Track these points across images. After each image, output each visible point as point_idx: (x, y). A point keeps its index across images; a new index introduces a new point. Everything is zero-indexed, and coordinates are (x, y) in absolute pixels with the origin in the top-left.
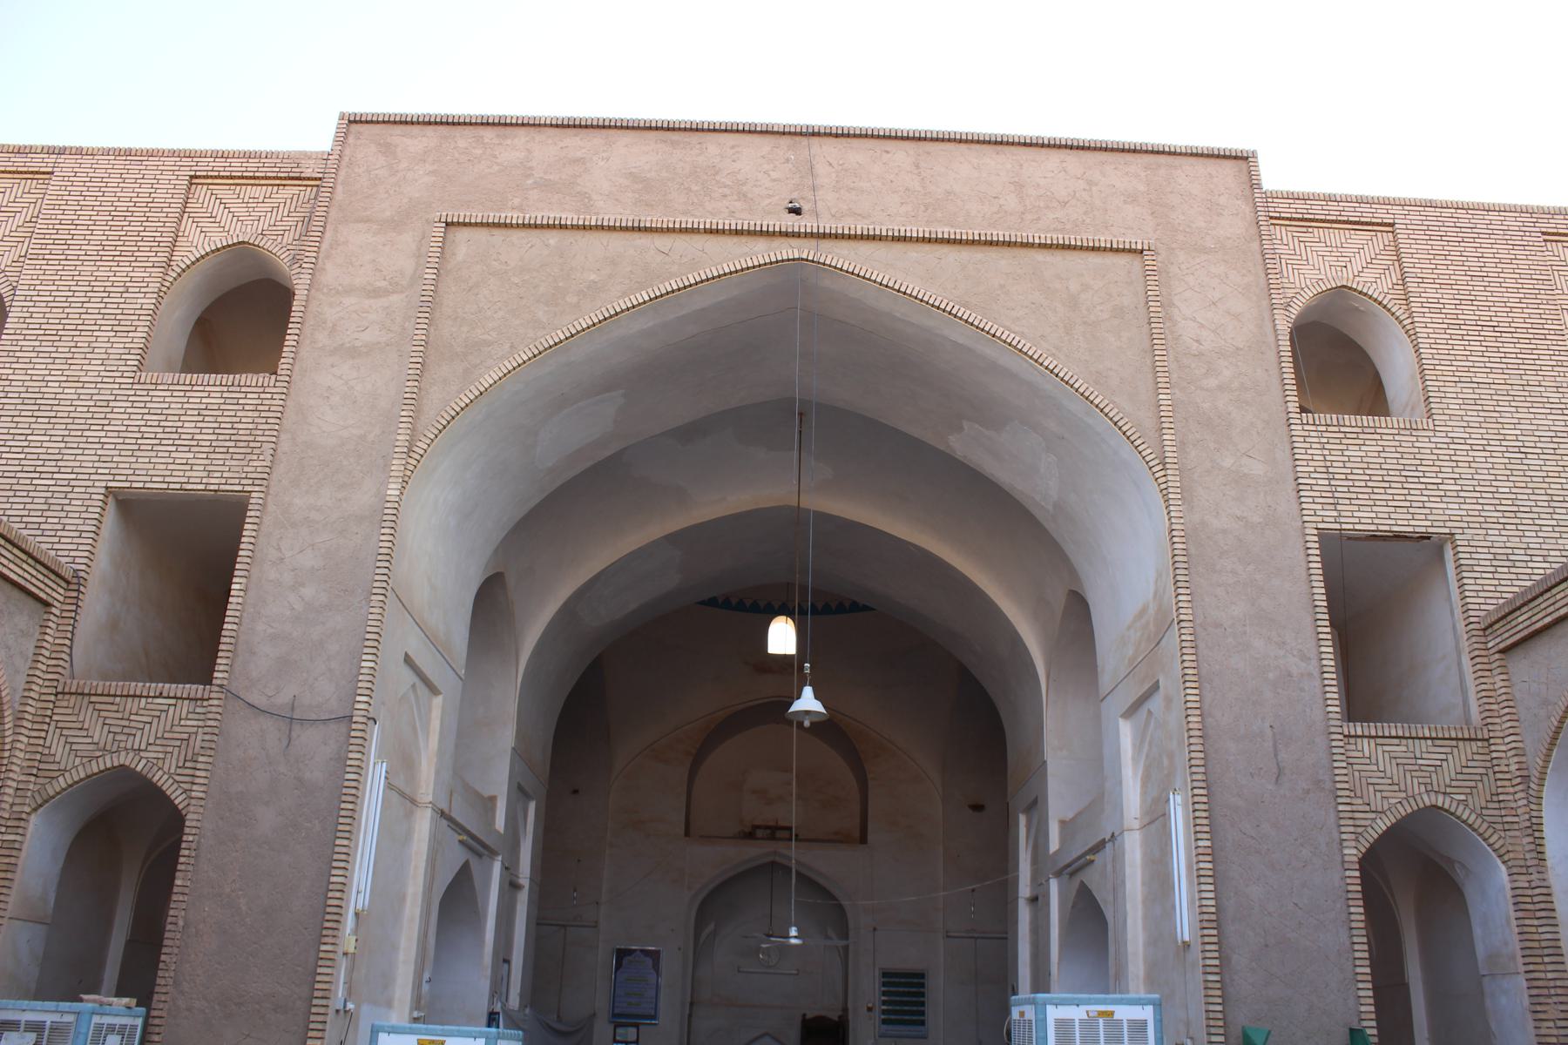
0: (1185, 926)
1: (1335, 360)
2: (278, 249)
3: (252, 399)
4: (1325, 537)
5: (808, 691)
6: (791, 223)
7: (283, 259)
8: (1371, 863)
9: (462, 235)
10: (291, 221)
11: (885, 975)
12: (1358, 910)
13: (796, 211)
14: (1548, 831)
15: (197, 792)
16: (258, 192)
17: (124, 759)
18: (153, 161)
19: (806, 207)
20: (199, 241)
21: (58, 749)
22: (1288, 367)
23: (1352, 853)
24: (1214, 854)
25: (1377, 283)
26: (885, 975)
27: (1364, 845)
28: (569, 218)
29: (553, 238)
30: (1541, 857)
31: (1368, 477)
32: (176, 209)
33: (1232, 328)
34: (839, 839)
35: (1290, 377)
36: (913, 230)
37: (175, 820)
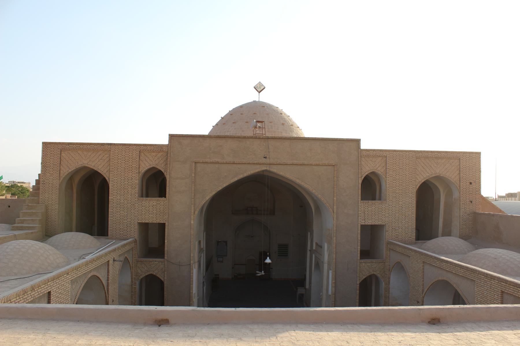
0: (330, 293)
1: (370, 187)
2: (161, 168)
3: (162, 203)
4: (362, 226)
5: (268, 258)
6: (264, 161)
7: (163, 171)
8: (361, 284)
9: (198, 165)
10: (162, 161)
11: (162, 227)
12: (358, 292)
13: (265, 158)
14: (391, 279)
15: (165, 278)
16: (154, 154)
17: (151, 273)
18: (131, 147)
19: (267, 157)
20: (145, 166)
21: (139, 271)
22: (360, 191)
23: (358, 282)
24: (335, 283)
25: (380, 171)
26: (162, 227)
27: (361, 281)
28: (219, 160)
29: (217, 166)
30: (389, 283)
31: (371, 213)
32: (138, 159)
33: (351, 182)
34: (226, 245)
35: (360, 193)
36: (289, 162)
37: (162, 283)
